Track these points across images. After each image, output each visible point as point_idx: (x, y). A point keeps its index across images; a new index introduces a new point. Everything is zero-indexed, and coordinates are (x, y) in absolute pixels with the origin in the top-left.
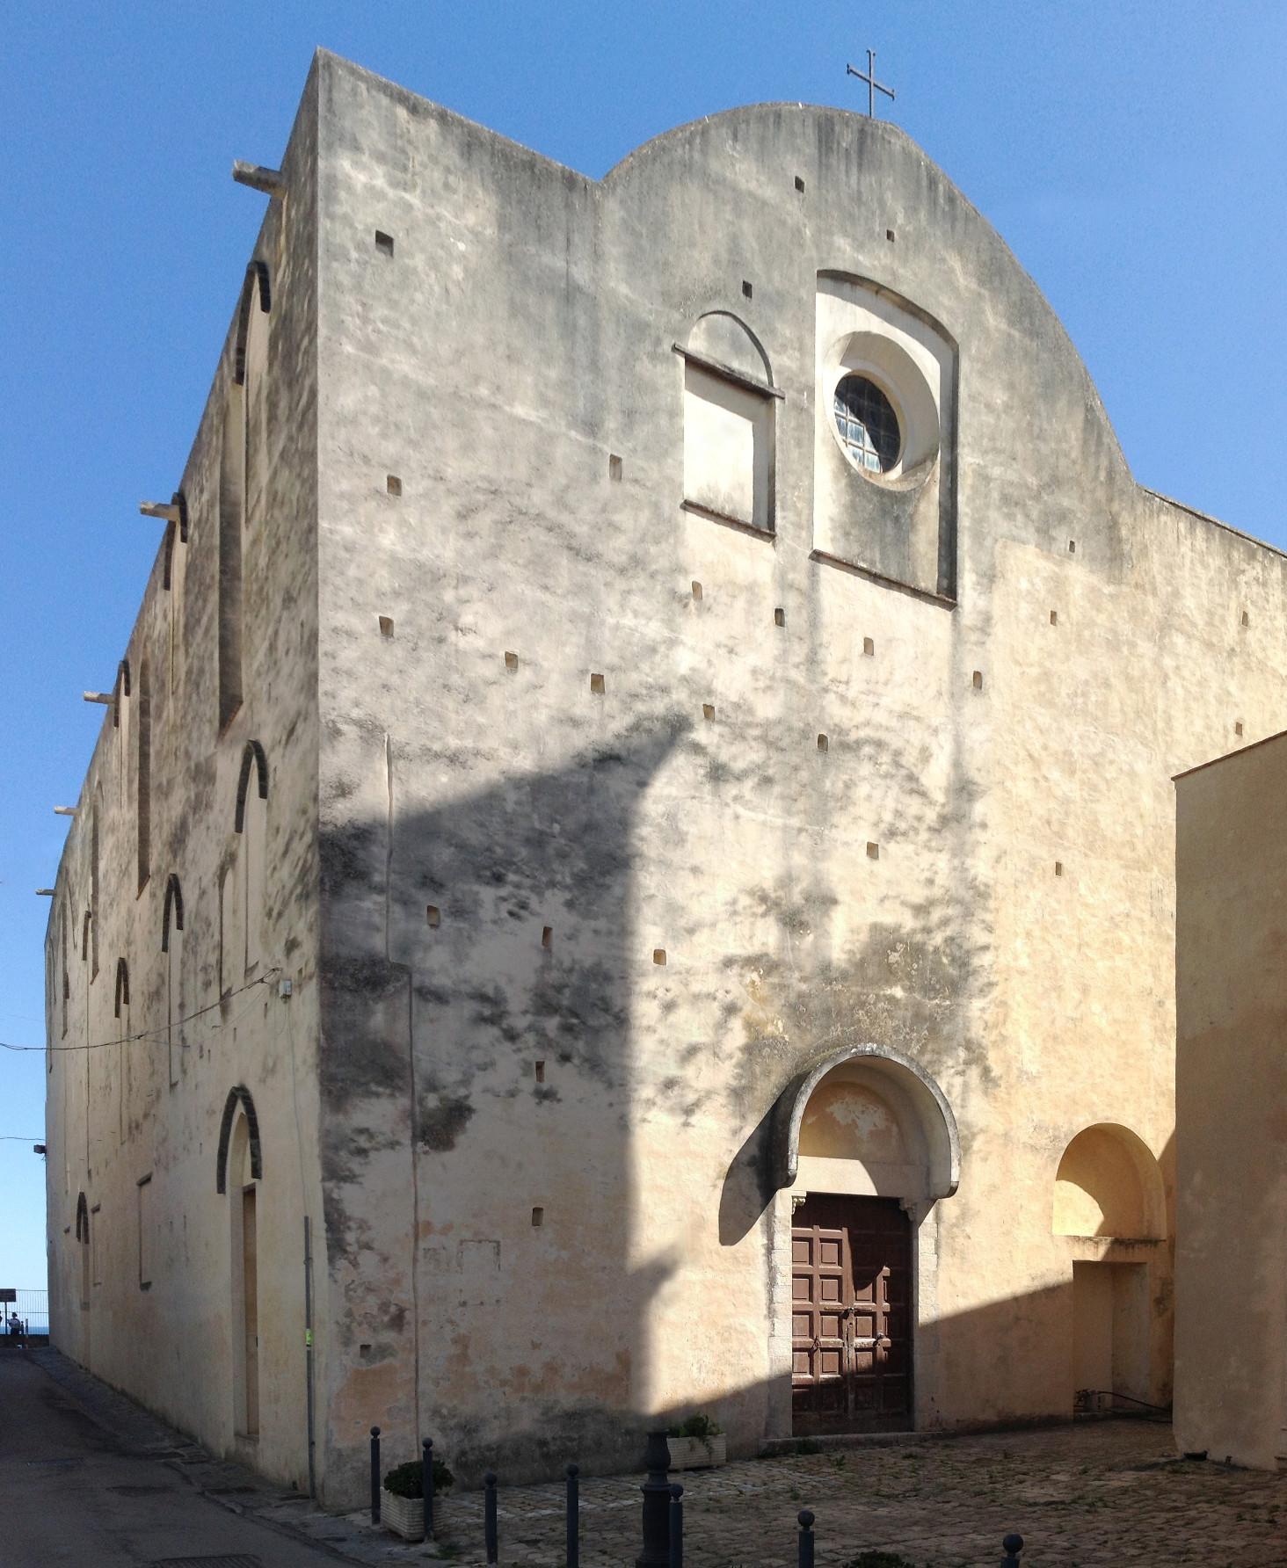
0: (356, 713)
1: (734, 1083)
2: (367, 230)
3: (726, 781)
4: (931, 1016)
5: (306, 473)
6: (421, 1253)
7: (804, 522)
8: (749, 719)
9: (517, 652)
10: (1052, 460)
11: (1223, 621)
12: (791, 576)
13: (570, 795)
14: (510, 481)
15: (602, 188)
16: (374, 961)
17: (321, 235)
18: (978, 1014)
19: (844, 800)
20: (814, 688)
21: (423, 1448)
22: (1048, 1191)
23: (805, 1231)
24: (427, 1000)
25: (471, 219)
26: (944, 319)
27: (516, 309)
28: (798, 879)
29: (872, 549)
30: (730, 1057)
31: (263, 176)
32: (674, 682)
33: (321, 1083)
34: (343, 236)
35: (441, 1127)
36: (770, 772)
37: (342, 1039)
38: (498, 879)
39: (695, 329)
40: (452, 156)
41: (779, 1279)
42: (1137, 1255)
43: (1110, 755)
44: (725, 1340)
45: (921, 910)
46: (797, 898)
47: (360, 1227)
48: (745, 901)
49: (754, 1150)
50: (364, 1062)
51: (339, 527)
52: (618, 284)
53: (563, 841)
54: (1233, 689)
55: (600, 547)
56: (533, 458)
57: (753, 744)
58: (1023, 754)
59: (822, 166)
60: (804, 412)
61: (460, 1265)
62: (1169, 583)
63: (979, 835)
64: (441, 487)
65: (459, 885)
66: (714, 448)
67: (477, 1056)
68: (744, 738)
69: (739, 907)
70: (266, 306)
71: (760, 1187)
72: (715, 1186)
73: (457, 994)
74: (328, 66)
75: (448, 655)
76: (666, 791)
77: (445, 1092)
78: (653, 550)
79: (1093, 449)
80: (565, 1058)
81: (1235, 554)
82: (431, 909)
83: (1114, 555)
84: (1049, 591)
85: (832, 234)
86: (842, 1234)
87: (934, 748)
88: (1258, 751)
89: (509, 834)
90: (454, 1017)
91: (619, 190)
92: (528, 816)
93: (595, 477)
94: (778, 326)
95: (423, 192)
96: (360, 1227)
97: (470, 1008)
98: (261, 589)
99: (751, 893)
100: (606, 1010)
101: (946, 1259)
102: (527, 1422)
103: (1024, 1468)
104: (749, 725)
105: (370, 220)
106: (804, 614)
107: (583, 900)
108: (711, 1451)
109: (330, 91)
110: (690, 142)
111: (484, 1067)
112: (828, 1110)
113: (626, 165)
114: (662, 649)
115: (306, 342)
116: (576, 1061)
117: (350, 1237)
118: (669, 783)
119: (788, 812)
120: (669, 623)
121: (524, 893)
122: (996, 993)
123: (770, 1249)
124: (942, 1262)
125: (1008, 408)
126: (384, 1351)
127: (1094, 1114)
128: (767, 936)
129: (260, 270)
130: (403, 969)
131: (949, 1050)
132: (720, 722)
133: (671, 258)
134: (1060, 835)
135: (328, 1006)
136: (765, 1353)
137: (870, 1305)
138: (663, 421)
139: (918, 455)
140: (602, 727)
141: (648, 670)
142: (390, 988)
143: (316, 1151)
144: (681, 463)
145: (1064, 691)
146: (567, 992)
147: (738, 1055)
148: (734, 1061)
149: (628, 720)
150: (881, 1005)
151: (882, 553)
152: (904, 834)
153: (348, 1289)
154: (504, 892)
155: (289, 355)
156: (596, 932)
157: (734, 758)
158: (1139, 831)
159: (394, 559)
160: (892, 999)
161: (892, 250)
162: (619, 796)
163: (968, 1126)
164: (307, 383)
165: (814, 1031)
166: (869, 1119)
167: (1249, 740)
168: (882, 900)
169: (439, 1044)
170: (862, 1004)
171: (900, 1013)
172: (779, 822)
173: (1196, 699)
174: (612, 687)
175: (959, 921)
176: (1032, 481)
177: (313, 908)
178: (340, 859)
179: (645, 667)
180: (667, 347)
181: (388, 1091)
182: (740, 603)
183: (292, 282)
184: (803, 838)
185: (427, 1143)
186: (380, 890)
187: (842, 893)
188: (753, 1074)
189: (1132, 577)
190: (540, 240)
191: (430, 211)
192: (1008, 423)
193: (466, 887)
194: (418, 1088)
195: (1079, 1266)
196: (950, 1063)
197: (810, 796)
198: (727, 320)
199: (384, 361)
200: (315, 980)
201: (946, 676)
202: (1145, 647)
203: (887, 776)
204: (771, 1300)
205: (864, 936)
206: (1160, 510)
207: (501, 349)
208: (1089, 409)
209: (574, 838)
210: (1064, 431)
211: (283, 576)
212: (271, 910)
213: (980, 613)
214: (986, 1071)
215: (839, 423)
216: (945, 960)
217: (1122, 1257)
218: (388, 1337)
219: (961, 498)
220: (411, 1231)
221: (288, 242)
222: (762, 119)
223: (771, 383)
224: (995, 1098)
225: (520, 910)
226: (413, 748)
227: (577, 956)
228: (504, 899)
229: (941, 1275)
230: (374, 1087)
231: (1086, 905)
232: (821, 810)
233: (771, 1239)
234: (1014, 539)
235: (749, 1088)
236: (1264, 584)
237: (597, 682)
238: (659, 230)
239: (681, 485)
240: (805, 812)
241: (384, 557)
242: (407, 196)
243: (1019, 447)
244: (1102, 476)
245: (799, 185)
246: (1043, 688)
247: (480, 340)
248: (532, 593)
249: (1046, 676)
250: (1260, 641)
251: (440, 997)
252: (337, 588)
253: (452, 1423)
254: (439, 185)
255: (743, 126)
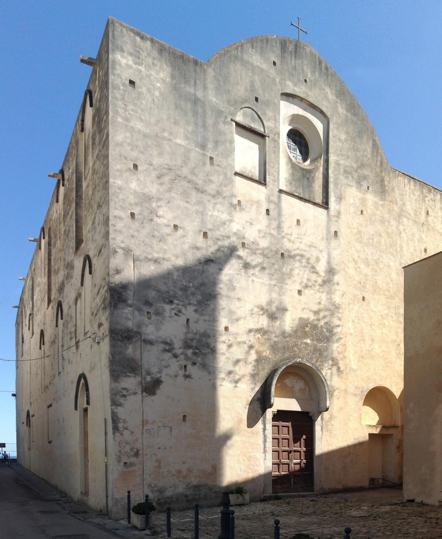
0: (122, 245)
1: (252, 372)
2: (126, 79)
3: (249, 268)
4: (320, 349)
5: (105, 163)
6: (144, 431)
7: (276, 179)
8: (257, 247)
9: (177, 224)
10: (361, 158)
11: (420, 213)
12: (271, 198)
13: (196, 273)
14: (175, 165)
15: (207, 65)
16: (128, 330)
17: (110, 81)
18: (336, 348)
19: (290, 275)
20: (279, 236)
21: (145, 498)
22: (360, 409)
23: (276, 423)
24: (147, 344)
25: (162, 75)
26: (324, 110)
27: (177, 106)
28: (274, 302)
29: (299, 189)
30: (251, 363)
31: (90, 61)
32: (231, 234)
33: (110, 372)
34: (118, 81)
35: (151, 387)
36: (265, 265)
37: (117, 357)
38: (171, 302)
39: (239, 113)
40: (155, 54)
41: (268, 440)
42: (391, 431)
43: (381, 260)
44: (249, 461)
45: (316, 313)
46: (274, 309)
47: (124, 422)
48: (256, 310)
49: (259, 395)
50: (125, 365)
51: (116, 181)
52: (212, 98)
53: (193, 289)
54: (423, 237)
55: (206, 188)
56: (183, 158)
57: (259, 256)
58: (351, 259)
59: (282, 57)
60: (276, 142)
61: (158, 435)
62: (401, 200)
63: (336, 287)
64: (152, 167)
65: (158, 304)
66: (245, 154)
67: (164, 363)
68: (256, 254)
69: (254, 312)
70: (91, 105)
71: (261, 408)
72: (245, 408)
73: (157, 342)
74: (113, 23)
75: (154, 225)
76: (229, 272)
77: (153, 375)
78: (224, 189)
79: (375, 154)
80: (194, 364)
81: (424, 191)
82: (148, 313)
83: (382, 191)
84: (360, 203)
85: (286, 80)
86: (289, 424)
87: (321, 257)
88: (432, 258)
89: (175, 287)
90: (156, 350)
91: (213, 65)
92: (181, 281)
93: (204, 164)
94: (267, 112)
95: (145, 66)
96: (124, 422)
97: (162, 346)
98: (90, 202)
99: (258, 307)
100: (208, 347)
101: (325, 433)
102: (181, 489)
103: (352, 505)
104: (257, 249)
105: (127, 76)
106: (276, 211)
107: (200, 309)
108: (244, 499)
109: (113, 31)
110: (237, 49)
111: (166, 367)
112: (284, 382)
113: (215, 57)
114: (227, 223)
115: (105, 117)
116: (198, 365)
117: (120, 425)
118: (230, 269)
119: (271, 279)
120: (230, 214)
121: (180, 307)
122: (342, 341)
123: (264, 429)
124: (324, 434)
125: (346, 140)
126: (132, 464)
127: (376, 383)
128: (263, 322)
129: (89, 93)
130: (139, 333)
131: (326, 361)
132: (247, 248)
133: (230, 89)
134: (364, 287)
135: (113, 346)
136: (263, 465)
137: (299, 449)
138: (228, 145)
139: (315, 156)
140: (207, 250)
141: (222, 230)
142: (134, 340)
143: (109, 396)
144: (234, 159)
145: (365, 238)
146: (195, 341)
147: (254, 363)
148: (252, 365)
149: (216, 247)
150: (303, 345)
151: (303, 190)
152: (311, 287)
153: (119, 443)
154: (173, 307)
155: (99, 122)
156: (205, 320)
157: (252, 261)
158: (391, 286)
159: (135, 192)
160: (306, 344)
161: (306, 86)
162: (213, 274)
163: (333, 387)
164: (106, 132)
165: (280, 354)
166: (299, 385)
167: (429, 254)
168: (303, 310)
169: (151, 359)
170: (296, 345)
171: (309, 348)
172: (268, 282)
173: (411, 240)
174: (210, 236)
175: (329, 317)
176: (355, 165)
177: (108, 312)
178: (117, 295)
179: (222, 229)
180: (229, 119)
181: (133, 375)
182: (254, 207)
183: (100, 97)
184: (276, 288)
185: (147, 393)
186: (131, 306)
187: (289, 307)
188: (259, 369)
189: (389, 198)
190: (185, 83)
191: (148, 72)
192: (346, 146)
193: (160, 305)
194: (144, 374)
195: (371, 435)
196: (326, 365)
197: (278, 274)
198: (250, 110)
199: (132, 124)
200: (108, 337)
201: (325, 232)
202: (393, 222)
203: (304, 267)
204: (265, 447)
205: (297, 322)
206: (398, 175)
207: (172, 120)
208: (374, 141)
209: (197, 288)
210: (366, 148)
211: (97, 198)
212: (93, 313)
213: (337, 211)
214: (339, 368)
215: (288, 146)
216: (324, 330)
217: (385, 432)
218: (133, 460)
219: (330, 171)
220: (141, 423)
221: (99, 83)
222: (262, 41)
223: (265, 132)
224: (342, 378)
225: (178, 313)
226: (142, 257)
227: (198, 329)
228: (173, 309)
229: (323, 438)
230: (128, 374)
231: (373, 311)
232: (282, 279)
233: (265, 426)
234: (348, 185)
235: (257, 374)
236: (434, 201)
237: (205, 235)
238: (226, 79)
239: (234, 167)
240: (277, 279)
241: (132, 191)
242: (140, 67)
243: (350, 153)
244: (379, 164)
245: (274, 63)
246: (358, 236)
247: (165, 117)
248: (183, 204)
249: (359, 232)
250: (433, 220)
251: (151, 343)
252: (116, 202)
253: (155, 489)
254: (151, 64)
255: (255, 43)
